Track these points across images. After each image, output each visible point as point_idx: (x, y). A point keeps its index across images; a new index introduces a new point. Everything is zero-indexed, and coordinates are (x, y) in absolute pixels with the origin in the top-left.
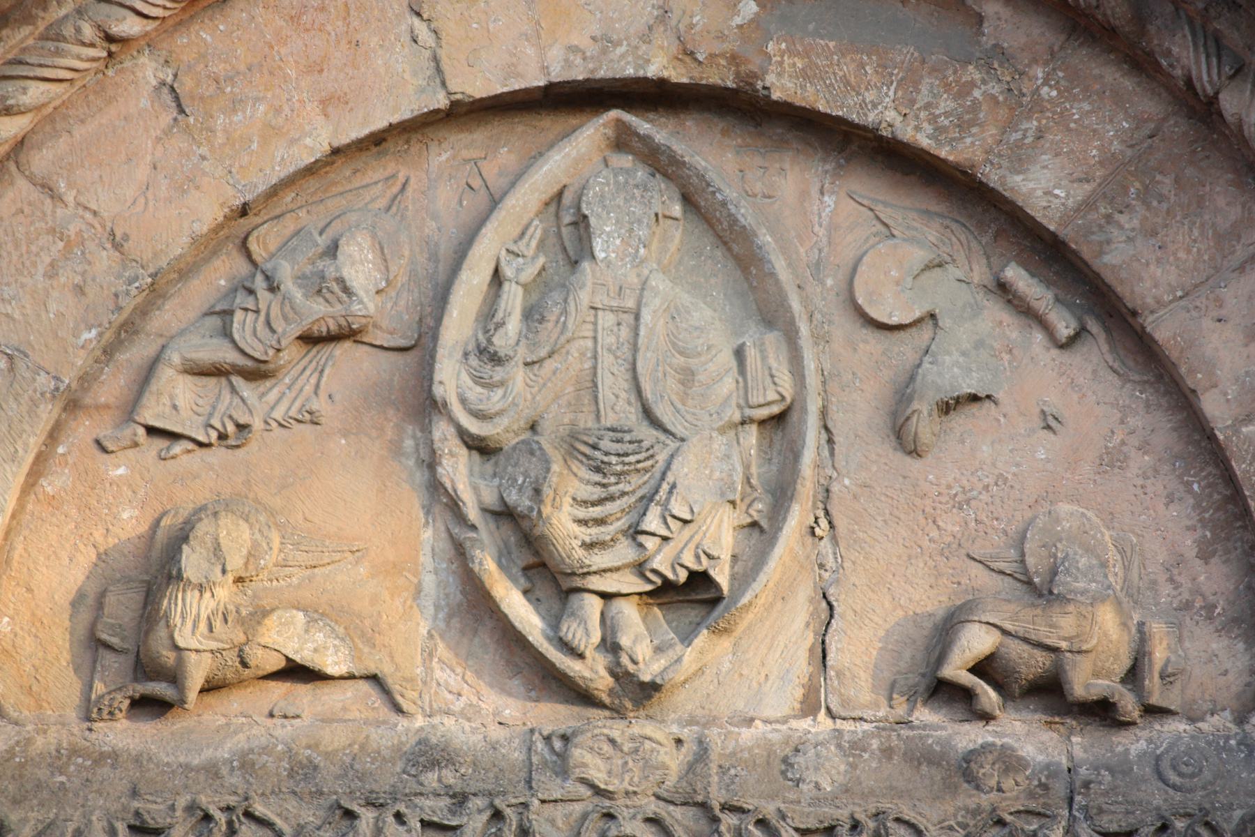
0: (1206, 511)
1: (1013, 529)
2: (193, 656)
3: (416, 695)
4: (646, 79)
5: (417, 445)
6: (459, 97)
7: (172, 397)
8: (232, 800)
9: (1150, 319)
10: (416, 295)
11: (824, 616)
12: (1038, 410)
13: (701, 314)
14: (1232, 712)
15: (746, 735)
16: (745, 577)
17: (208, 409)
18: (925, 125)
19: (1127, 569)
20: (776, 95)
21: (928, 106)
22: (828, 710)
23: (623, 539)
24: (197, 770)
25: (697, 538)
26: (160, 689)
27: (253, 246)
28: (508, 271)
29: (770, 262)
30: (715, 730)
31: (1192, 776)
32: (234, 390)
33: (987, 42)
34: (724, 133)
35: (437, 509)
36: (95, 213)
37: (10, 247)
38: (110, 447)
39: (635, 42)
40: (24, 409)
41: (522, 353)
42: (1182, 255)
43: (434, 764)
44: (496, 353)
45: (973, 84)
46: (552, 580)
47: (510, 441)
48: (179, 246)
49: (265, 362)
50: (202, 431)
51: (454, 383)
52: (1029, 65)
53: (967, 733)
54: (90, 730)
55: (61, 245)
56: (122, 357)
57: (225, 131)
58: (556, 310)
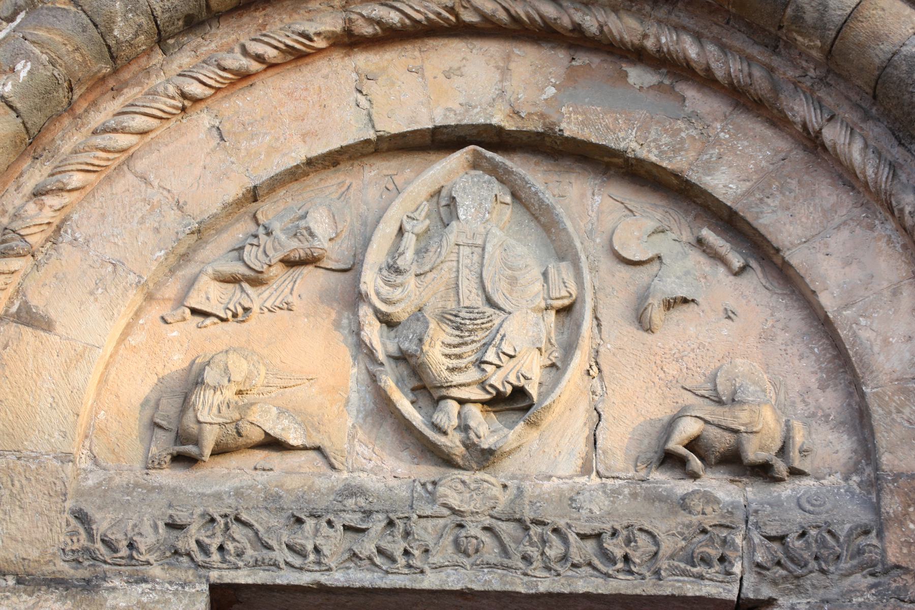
0: (822, 363)
1: (708, 373)
2: (208, 426)
3: (344, 459)
4: (491, 125)
5: (350, 323)
6: (382, 133)
7: (206, 293)
8: (228, 511)
9: (788, 253)
10: (353, 242)
11: (596, 419)
12: (722, 308)
13: (520, 249)
14: (841, 474)
15: (547, 485)
16: (548, 388)
17: (227, 300)
18: (654, 150)
19: (777, 394)
20: (567, 134)
21: (654, 141)
22: (598, 472)
23: (472, 367)
24: (209, 496)
25: (518, 368)
26: (190, 449)
27: (260, 216)
28: (407, 227)
29: (563, 222)
30: (528, 483)
31: (820, 506)
32: (243, 290)
33: (688, 110)
34: (536, 164)
35: (361, 357)
36: (169, 191)
37: (120, 208)
38: (169, 320)
39: (485, 106)
40: (120, 292)
41: (415, 269)
42: (804, 220)
43: (352, 494)
44: (398, 268)
45: (681, 130)
46: (429, 392)
47: (403, 317)
48: (215, 208)
49: (261, 272)
50: (223, 311)
51: (373, 284)
52: (712, 122)
53: (683, 485)
54: (147, 474)
55: (148, 207)
56: (180, 274)
57: (246, 149)
58: (435, 246)
